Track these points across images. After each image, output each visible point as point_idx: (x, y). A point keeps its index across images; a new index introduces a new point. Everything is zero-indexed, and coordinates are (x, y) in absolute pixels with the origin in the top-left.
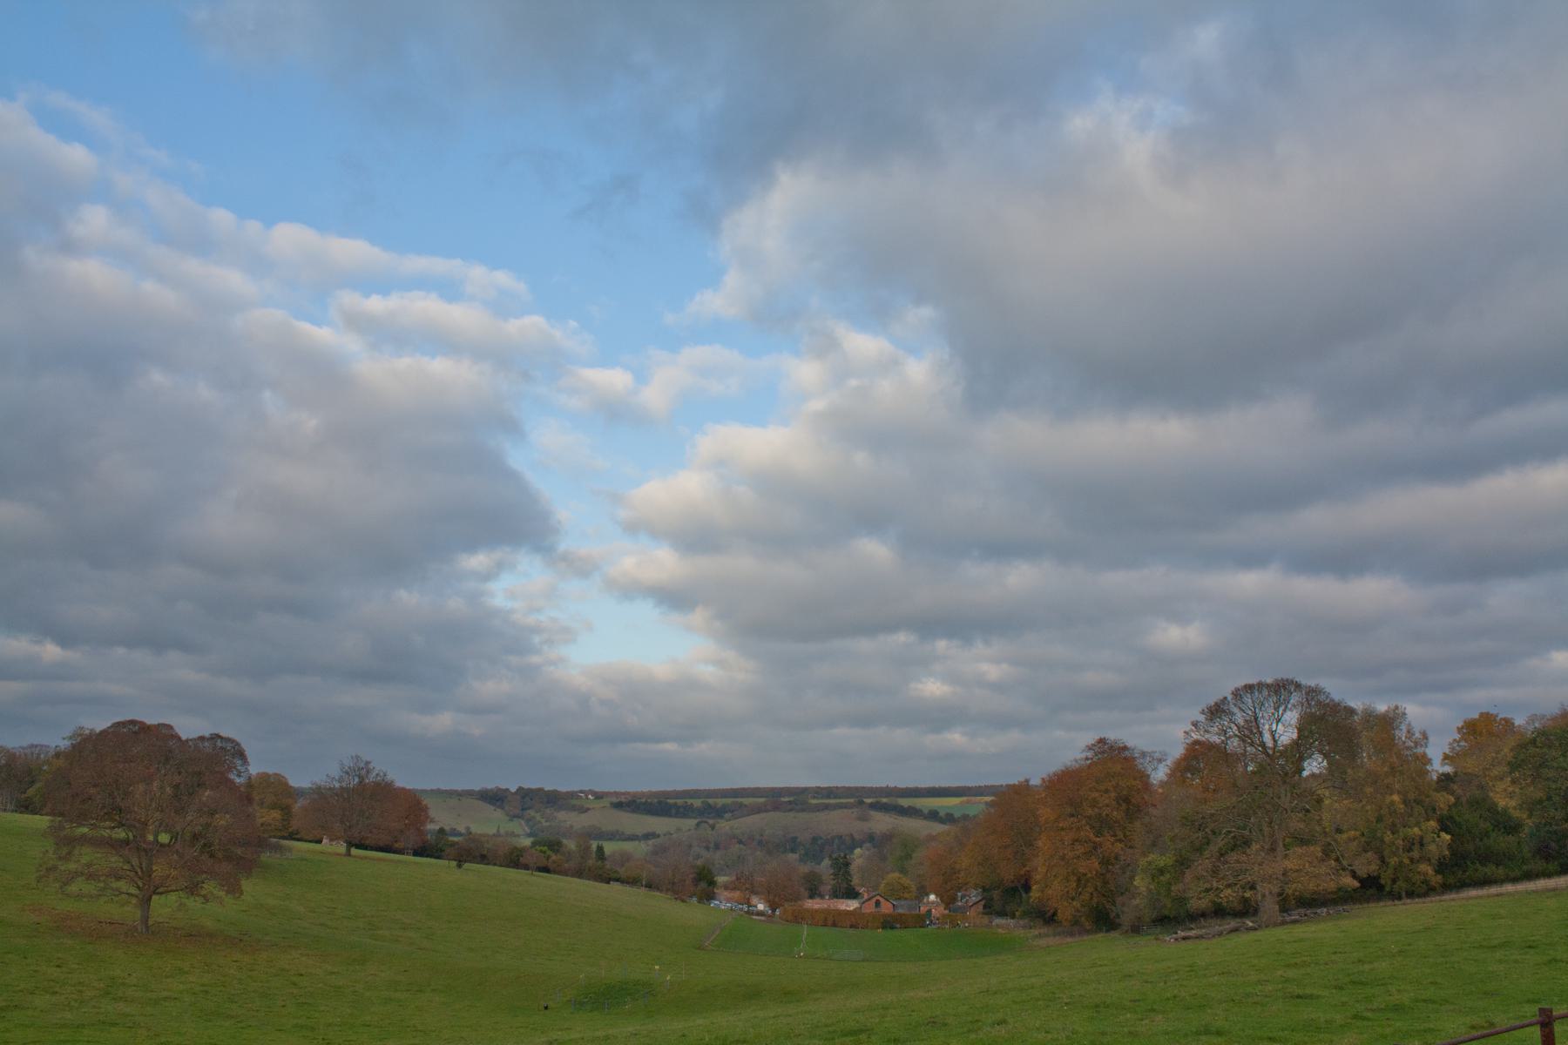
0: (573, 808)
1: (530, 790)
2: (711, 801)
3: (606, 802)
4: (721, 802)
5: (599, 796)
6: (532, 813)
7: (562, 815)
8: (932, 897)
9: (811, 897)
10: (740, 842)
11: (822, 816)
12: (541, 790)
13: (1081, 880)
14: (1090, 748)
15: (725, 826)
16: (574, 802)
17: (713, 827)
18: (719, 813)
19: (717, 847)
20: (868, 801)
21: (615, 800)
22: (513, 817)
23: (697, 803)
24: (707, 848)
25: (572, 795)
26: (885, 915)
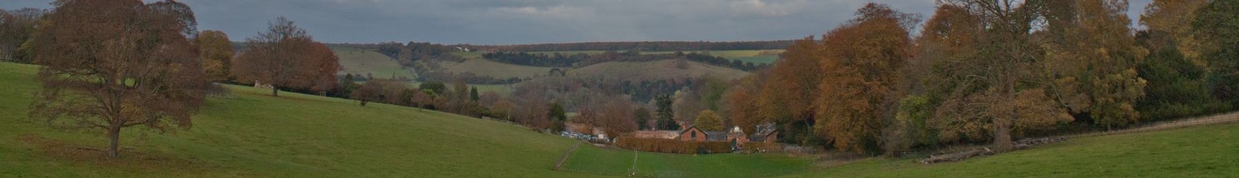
0: (453, 59)
1: (419, 44)
2: (561, 53)
3: (479, 54)
4: (569, 53)
5: (473, 49)
6: (420, 62)
7: (444, 64)
8: (737, 129)
9: (641, 129)
10: (585, 85)
11: (649, 64)
12: (427, 44)
13: (854, 116)
14: (861, 11)
15: (572, 72)
16: (453, 54)
17: (563, 74)
18: (568, 62)
19: (567, 89)
20: (686, 53)
21: (486, 52)
22: (405, 66)
23: (551, 54)
24: (559, 91)
25: (452, 48)
26: (699, 143)
